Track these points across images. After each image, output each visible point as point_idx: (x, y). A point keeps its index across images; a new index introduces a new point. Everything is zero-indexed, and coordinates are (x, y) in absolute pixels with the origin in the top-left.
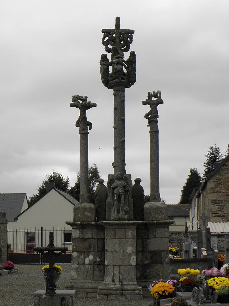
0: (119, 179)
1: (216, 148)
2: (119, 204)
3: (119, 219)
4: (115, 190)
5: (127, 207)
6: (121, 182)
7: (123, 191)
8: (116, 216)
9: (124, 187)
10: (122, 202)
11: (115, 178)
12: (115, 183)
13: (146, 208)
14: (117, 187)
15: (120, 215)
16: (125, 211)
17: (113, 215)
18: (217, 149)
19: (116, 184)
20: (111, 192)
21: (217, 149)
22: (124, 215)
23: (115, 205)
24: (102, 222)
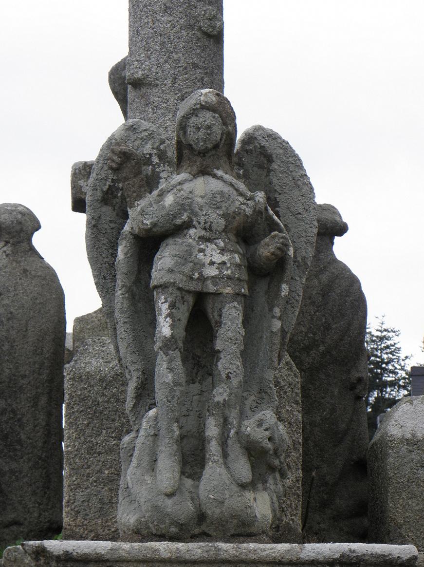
0: (203, 153)
1: (385, 330)
2: (195, 388)
3: (198, 526)
4: (165, 261)
5: (268, 415)
6: (214, 185)
7: (238, 266)
8: (170, 495)
9: (246, 233)
10: (229, 362)
11: (162, 155)
12: (161, 195)
13: (405, 441)
14: (178, 230)
15: (202, 487)
16: (255, 453)
17: (135, 489)
18: (390, 334)
19: (169, 200)
20: (119, 283)
21: (390, 334)
22: (243, 486)
23: (160, 394)
24: (40, 552)
